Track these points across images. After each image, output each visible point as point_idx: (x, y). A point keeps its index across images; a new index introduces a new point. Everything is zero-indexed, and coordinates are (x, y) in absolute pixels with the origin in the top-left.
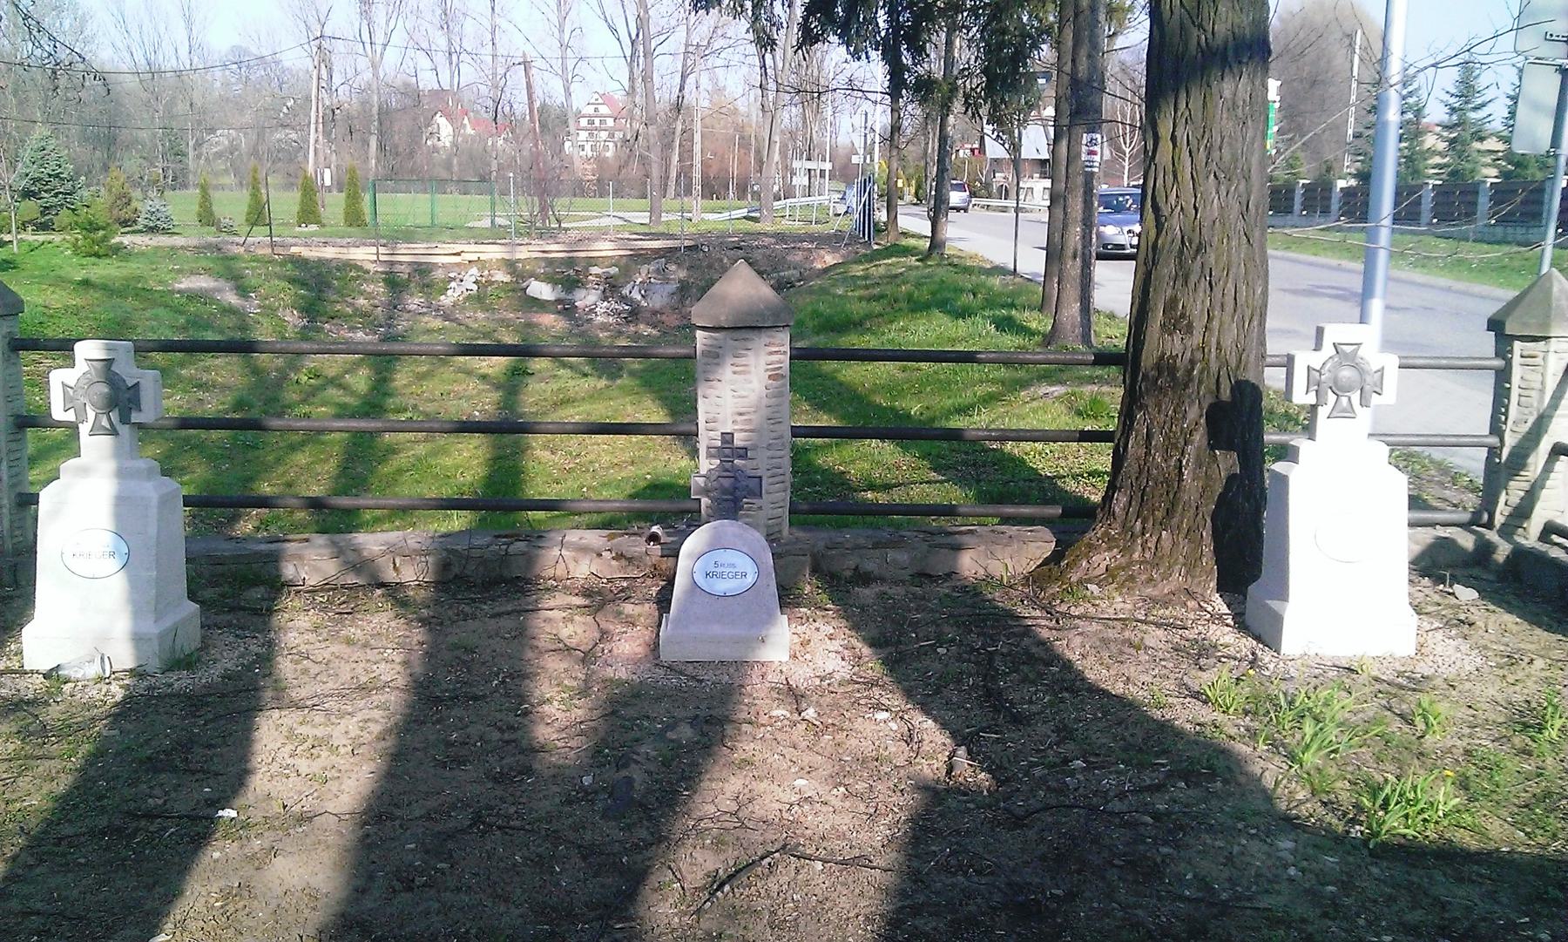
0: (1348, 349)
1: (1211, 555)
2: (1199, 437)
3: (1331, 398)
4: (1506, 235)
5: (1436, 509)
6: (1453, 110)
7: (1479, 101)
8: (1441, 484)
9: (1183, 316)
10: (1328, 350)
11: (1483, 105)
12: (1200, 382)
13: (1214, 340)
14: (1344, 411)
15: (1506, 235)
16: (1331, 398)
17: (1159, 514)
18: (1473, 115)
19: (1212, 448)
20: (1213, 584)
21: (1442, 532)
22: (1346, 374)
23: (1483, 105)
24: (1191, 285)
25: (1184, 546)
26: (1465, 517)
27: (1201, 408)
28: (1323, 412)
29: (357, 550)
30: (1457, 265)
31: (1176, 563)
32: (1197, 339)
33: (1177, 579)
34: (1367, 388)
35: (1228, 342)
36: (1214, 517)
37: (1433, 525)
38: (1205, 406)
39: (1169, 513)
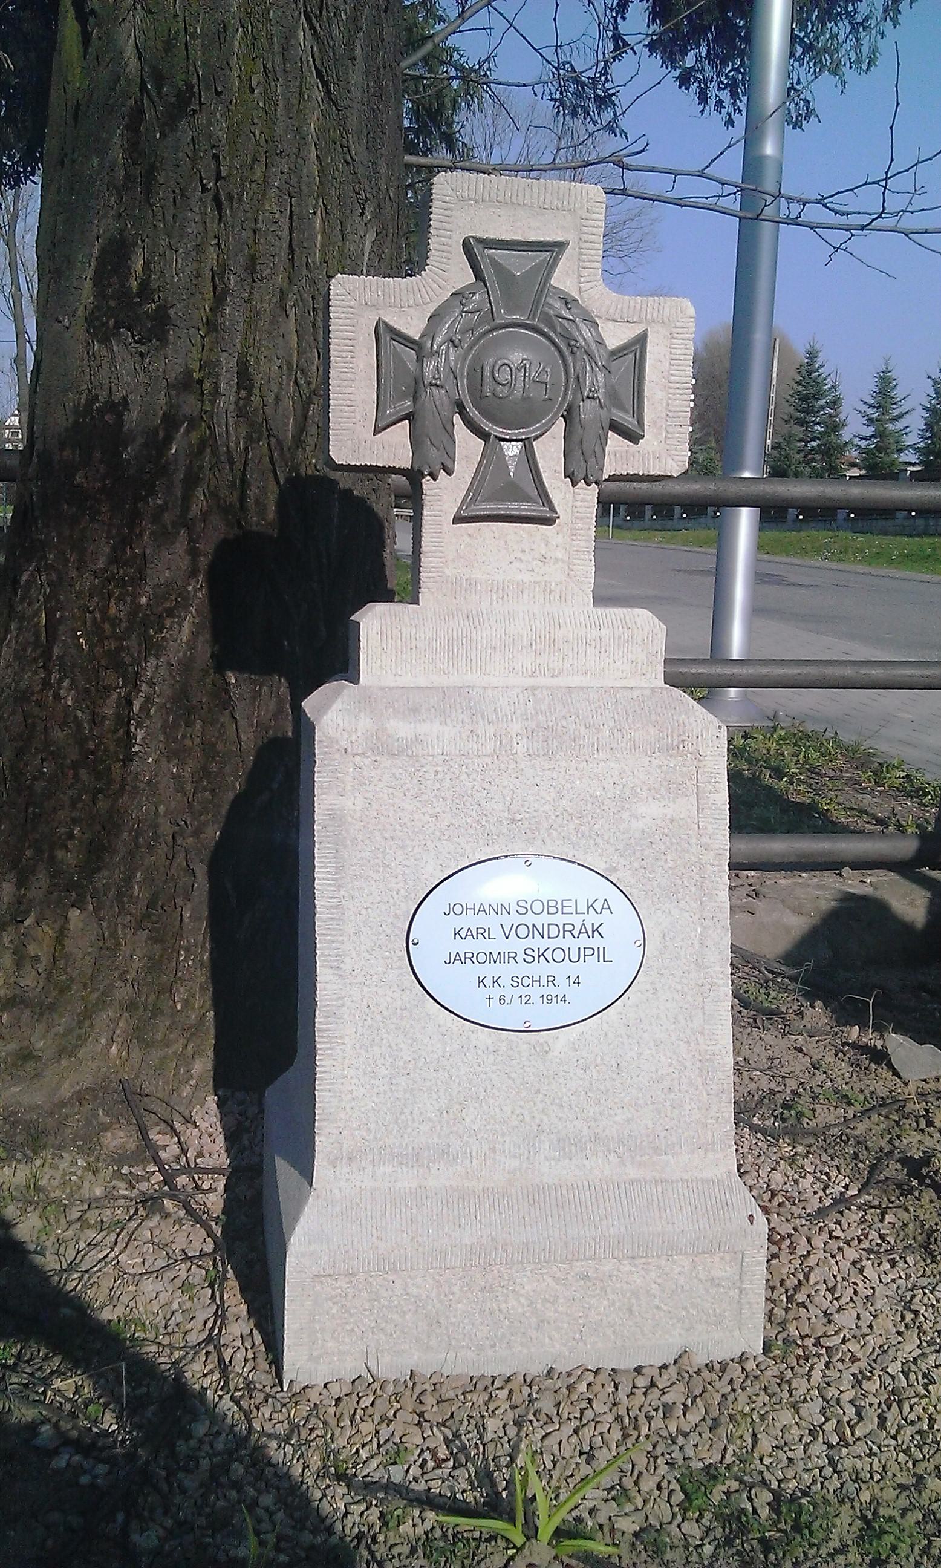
0: (518, 264)
1: (202, 976)
2: (186, 633)
3: (467, 447)
4: (927, 526)
5: (844, 830)
6: (871, 421)
7: (896, 413)
8: (856, 784)
9: (145, 288)
10: (446, 271)
11: (901, 416)
12: (192, 481)
13: (228, 363)
14: (513, 492)
15: (927, 526)
16: (467, 447)
17: (69, 858)
18: (890, 426)
19: (221, 663)
20: (203, 1066)
21: (855, 883)
22: (520, 359)
23: (901, 416)
24: (162, 195)
25: (135, 950)
26: (906, 847)
27: (193, 553)
28: (443, 496)
29: (33, 872)
30: (879, 557)
31: (102, 1003)
32: (181, 353)
33: (107, 1052)
34: (587, 410)
35: (268, 370)
36: (219, 863)
37: (835, 865)
38: (207, 548)
39: (96, 853)
